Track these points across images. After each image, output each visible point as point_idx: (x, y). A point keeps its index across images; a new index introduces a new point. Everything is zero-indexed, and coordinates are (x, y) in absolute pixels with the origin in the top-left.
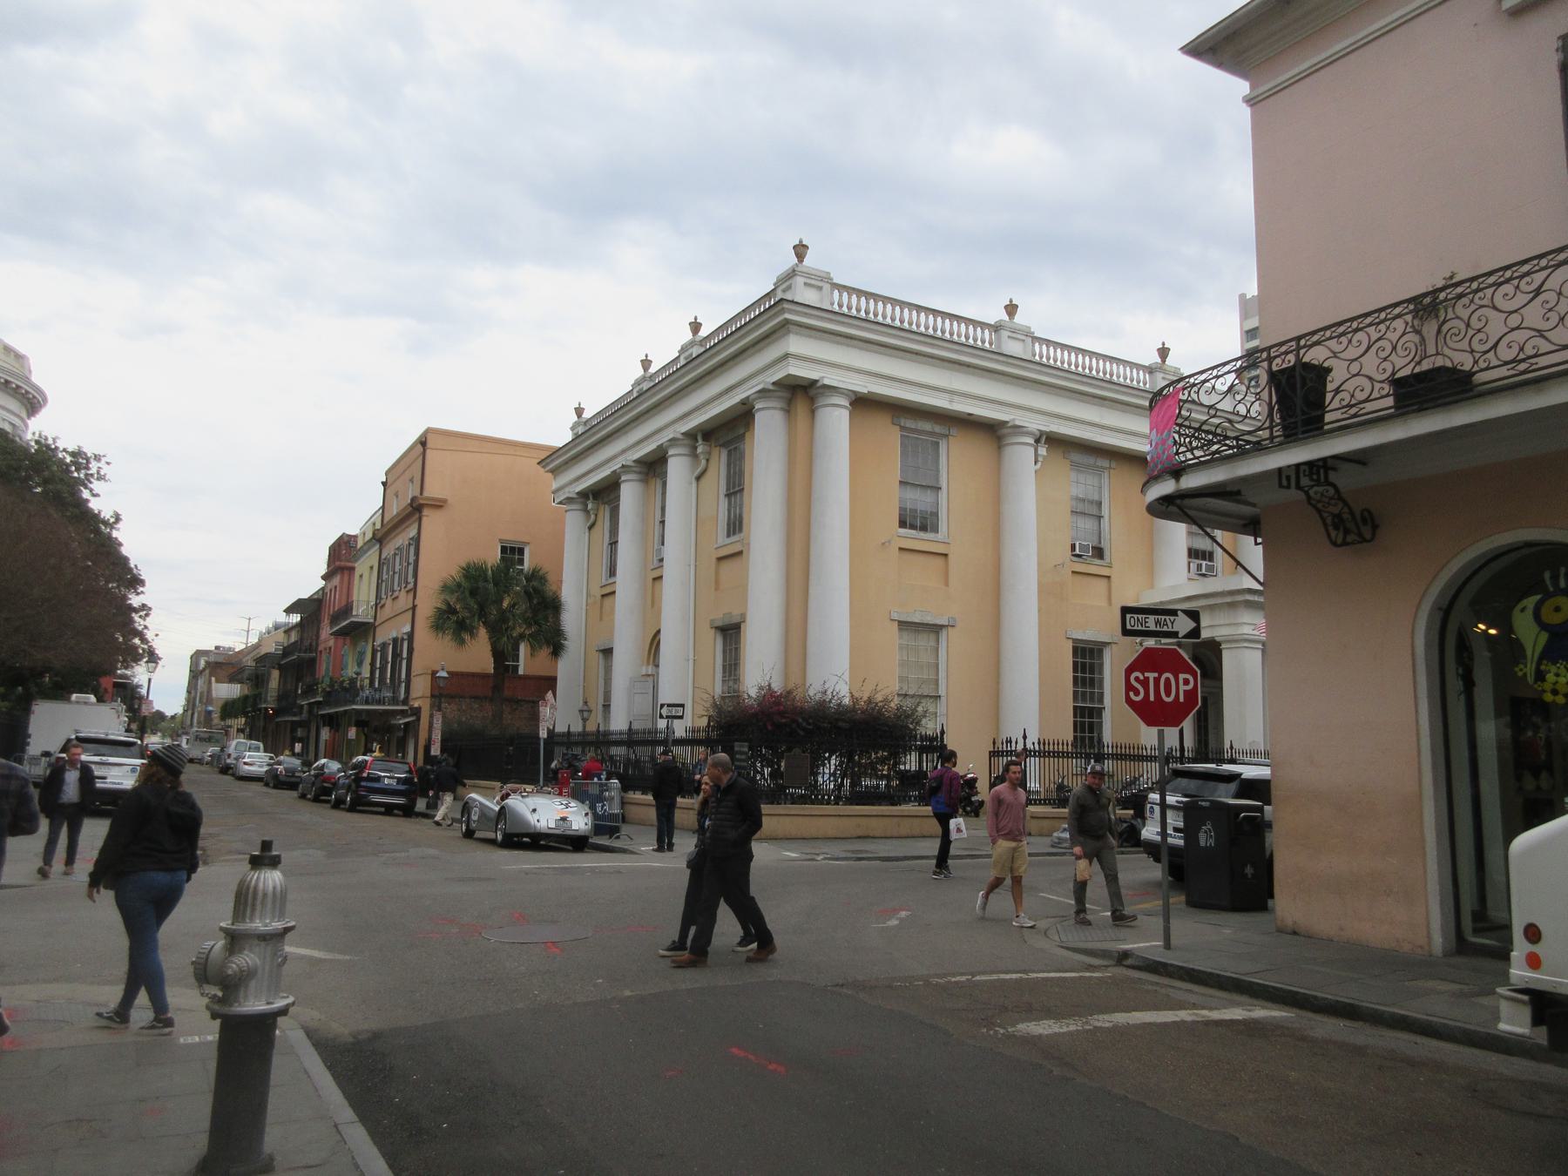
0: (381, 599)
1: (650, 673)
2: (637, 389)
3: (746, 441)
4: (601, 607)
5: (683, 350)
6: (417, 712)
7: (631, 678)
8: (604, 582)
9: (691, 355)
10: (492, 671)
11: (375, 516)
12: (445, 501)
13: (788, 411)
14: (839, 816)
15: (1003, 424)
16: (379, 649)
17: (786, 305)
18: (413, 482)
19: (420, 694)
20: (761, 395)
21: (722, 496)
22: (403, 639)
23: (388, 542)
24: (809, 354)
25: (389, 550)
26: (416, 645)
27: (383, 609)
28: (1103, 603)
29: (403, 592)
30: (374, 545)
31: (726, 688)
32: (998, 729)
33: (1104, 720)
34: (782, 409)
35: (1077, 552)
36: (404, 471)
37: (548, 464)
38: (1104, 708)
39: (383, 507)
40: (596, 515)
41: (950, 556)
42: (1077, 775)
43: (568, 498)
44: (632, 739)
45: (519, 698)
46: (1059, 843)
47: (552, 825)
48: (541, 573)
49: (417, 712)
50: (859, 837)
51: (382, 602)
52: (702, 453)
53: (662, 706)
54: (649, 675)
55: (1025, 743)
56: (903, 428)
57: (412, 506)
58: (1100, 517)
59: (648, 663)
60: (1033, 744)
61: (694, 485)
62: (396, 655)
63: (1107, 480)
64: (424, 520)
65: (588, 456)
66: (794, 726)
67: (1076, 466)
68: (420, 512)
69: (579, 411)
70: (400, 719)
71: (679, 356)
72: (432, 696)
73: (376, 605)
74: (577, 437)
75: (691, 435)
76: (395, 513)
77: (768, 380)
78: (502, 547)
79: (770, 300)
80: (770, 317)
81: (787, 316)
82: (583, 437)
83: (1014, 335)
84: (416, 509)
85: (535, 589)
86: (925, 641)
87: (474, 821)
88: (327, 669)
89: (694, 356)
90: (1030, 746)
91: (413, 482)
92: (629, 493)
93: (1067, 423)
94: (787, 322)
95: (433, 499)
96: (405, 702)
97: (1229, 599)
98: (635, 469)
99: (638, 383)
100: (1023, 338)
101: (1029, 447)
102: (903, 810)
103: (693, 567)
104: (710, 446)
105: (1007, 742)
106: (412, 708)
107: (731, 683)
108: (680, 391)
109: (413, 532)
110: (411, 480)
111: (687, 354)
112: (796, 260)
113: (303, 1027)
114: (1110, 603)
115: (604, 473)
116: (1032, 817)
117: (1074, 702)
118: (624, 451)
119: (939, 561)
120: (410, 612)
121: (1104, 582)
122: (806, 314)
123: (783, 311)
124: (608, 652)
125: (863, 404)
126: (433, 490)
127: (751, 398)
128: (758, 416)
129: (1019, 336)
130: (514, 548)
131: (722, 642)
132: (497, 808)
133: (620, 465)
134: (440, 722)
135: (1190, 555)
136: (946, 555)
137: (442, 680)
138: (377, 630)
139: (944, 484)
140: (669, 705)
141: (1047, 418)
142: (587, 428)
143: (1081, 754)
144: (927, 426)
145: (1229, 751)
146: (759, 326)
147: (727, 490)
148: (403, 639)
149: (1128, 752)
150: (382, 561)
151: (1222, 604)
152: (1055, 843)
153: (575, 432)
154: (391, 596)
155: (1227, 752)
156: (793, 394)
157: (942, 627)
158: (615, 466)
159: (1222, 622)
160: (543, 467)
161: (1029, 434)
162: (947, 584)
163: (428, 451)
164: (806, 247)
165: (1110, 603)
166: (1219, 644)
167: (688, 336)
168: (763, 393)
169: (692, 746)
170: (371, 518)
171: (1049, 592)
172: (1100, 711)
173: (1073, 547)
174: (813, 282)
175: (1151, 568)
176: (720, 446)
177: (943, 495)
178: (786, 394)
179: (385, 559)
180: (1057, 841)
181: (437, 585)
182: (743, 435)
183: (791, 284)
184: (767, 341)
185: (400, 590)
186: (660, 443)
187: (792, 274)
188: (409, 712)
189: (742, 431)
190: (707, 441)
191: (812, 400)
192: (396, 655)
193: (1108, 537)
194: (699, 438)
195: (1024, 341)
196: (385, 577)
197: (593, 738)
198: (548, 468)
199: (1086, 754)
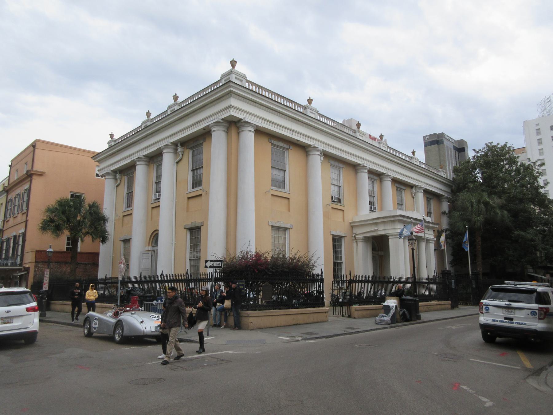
0: (7, 218)
1: (150, 250)
2: (144, 125)
3: (204, 145)
4: (123, 220)
5: (170, 107)
6: (27, 270)
7: (141, 252)
8: (124, 210)
9: (174, 109)
10: (65, 250)
11: (6, 180)
12: (44, 173)
13: (228, 132)
14: (286, 315)
15: (309, 146)
16: (5, 241)
17: (231, 84)
18: (27, 164)
19: (29, 261)
20: (215, 124)
21: (154, 184)
22: (19, 236)
23: (12, 192)
25: (12, 195)
26: (27, 238)
27: (8, 222)
28: (341, 220)
29: (20, 214)
30: (4, 194)
31: (192, 256)
33: (342, 267)
34: (225, 131)
35: (334, 200)
36: (22, 160)
37: (96, 158)
38: (342, 262)
39: (9, 177)
40: (120, 181)
41: (290, 199)
42: (335, 290)
43: (107, 173)
44: (141, 281)
45: (79, 262)
46: (381, 322)
47: (153, 330)
48: (96, 204)
49: (27, 270)
50: (294, 325)
51: (8, 219)
52: (180, 151)
53: (206, 262)
54: (149, 251)
55: (350, 277)
56: (273, 144)
57: (27, 174)
58: (339, 187)
59: (149, 246)
60: (353, 277)
61: (175, 165)
62: (15, 243)
63: (342, 173)
64: (33, 181)
65: (118, 154)
66: (266, 271)
67: (332, 166)
68: (31, 177)
69: (112, 136)
70: (18, 273)
71: (167, 110)
72: (36, 262)
73: (4, 221)
74: (110, 147)
75: (175, 144)
76: (16, 179)
77: (220, 117)
78: (71, 195)
79: (217, 85)
80: (222, 89)
81: (231, 89)
82: (113, 147)
83: (312, 111)
84: (29, 176)
85: (94, 212)
86: (280, 234)
87: (95, 328)
89: (175, 110)
91: (27, 164)
92: (140, 171)
94: (231, 92)
95: (36, 171)
96: (21, 265)
97: (393, 219)
98: (112, 174)
99: (144, 122)
100: (315, 113)
101: (318, 156)
102: (320, 310)
103: (174, 202)
104: (184, 149)
106: (25, 268)
107: (195, 253)
108: (171, 124)
109: (26, 186)
110: (26, 164)
111: (171, 109)
112: (231, 68)
115: (129, 161)
116: (356, 310)
117: (333, 260)
118: (138, 151)
119: (286, 201)
120: (25, 223)
121: (341, 212)
122: (239, 89)
123: (230, 86)
124: (127, 241)
125: (260, 132)
126: (38, 167)
127: (161, 148)
128: (213, 134)
129: (313, 112)
130: (77, 195)
131: (190, 235)
132: (113, 321)
133: (137, 157)
134: (48, 274)
135: (374, 203)
136: (288, 198)
137: (50, 253)
138: (4, 232)
139: (287, 169)
140: (211, 261)
141: (325, 145)
142: (116, 143)
143: (339, 282)
144: (281, 144)
146: (129, 141)
147: (192, 168)
148: (19, 236)
150: (8, 201)
151: (389, 221)
152: (379, 322)
153: (110, 144)
154: (21, 212)
156: (230, 125)
157: (287, 228)
158: (134, 157)
159: (389, 228)
160: (94, 159)
161: (319, 151)
162: (289, 211)
163: (36, 151)
164: (236, 62)
166: (388, 236)
167: (172, 101)
168: (217, 123)
169: (111, 284)
170: (2, 181)
171: (326, 216)
172: (341, 263)
173: (332, 197)
174: (239, 77)
175: (356, 207)
176: (189, 148)
177: (287, 174)
178: (226, 125)
179: (10, 200)
180: (380, 321)
181: (43, 208)
182: (133, 172)
183: (230, 77)
184: (220, 100)
185: (10, 218)
186: (159, 147)
187: (230, 72)
188: (23, 270)
189: (201, 142)
191: (238, 128)
192: (15, 243)
193: (342, 195)
195: (315, 114)
196: (9, 208)
197: (103, 281)
198: (96, 160)
199: (337, 281)
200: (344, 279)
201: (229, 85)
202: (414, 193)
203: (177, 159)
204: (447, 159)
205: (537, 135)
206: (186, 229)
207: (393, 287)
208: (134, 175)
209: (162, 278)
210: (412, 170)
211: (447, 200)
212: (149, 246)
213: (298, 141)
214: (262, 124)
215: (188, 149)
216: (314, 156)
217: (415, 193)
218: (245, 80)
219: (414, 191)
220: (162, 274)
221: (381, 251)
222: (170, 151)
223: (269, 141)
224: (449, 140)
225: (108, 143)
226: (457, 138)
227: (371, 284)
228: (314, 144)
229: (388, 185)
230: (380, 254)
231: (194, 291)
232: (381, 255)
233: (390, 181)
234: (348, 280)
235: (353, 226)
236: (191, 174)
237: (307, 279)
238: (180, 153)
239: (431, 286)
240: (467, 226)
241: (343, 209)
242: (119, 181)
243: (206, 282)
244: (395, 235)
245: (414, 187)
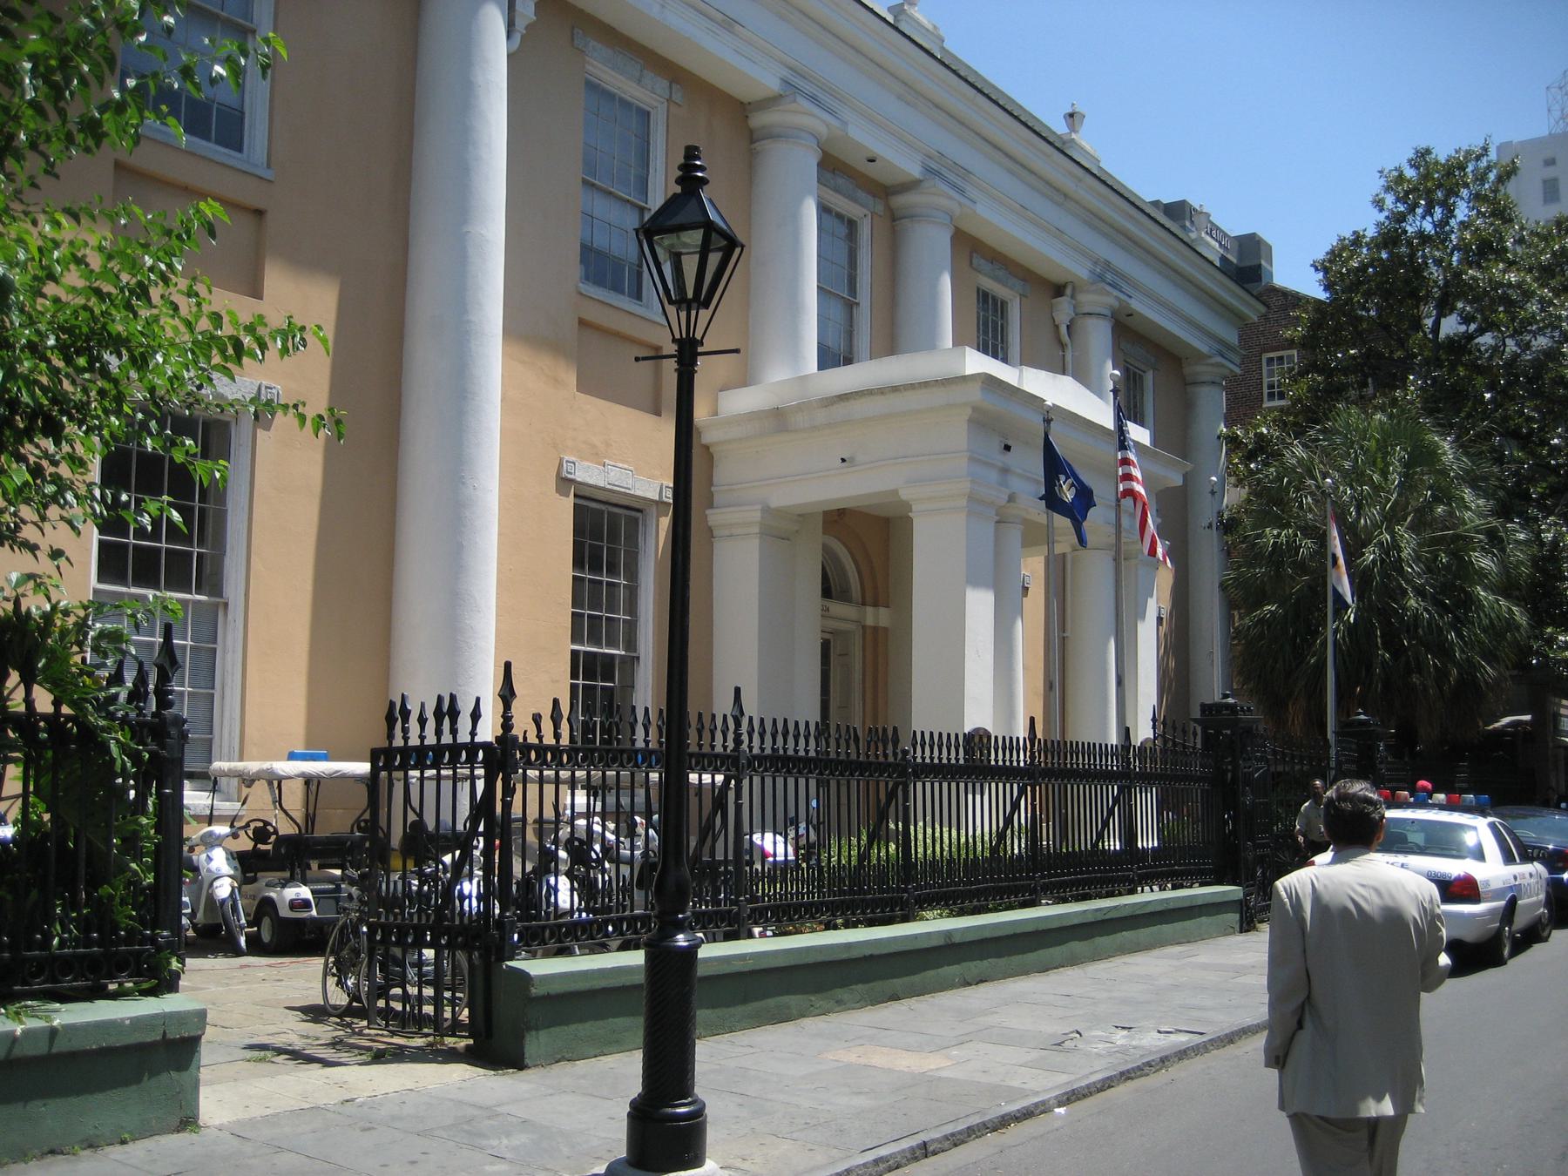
32: (875, 718)
38: (638, 658)
60: (537, 719)
88: (593, 66)
90: (522, 726)
105: (439, 715)
113: (1431, 880)
136: (259, 213)
149: (549, 740)
205: (1555, 180)
207: (888, 804)
221: (876, 605)
230: (870, 621)
232: (875, 629)
234: (486, 746)
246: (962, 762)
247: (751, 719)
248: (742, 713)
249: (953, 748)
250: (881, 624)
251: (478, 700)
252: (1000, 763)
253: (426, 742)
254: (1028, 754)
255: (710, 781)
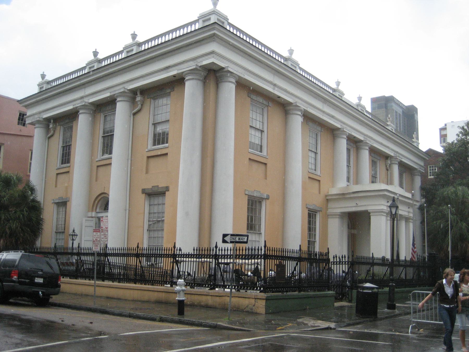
1: (93, 216)
13: (205, 81)
17: (216, 26)
21: (101, 138)
24: (93, 91)
28: (316, 191)
41: (268, 165)
54: (92, 217)
61: (132, 117)
93: (319, 111)
114: (320, 193)
119: (263, 167)
122: (227, 34)
123: (214, 29)
145: (215, 249)
155: (213, 250)
158: (78, 104)
161: (300, 110)
165: (320, 193)
166: (369, 213)
190: (142, 95)
194: (138, 93)
200: (345, 260)
201: (213, 27)
202: (388, 165)
203: (133, 110)
204: (402, 127)
206: (144, 194)
208: (73, 125)
209: (78, 251)
210: (390, 138)
211: (420, 174)
212: (92, 211)
213: (279, 97)
214: (244, 75)
215: (150, 99)
216: (295, 115)
217: (390, 165)
218: (227, 22)
219: (389, 162)
220: (138, 247)
222: (125, 100)
223: (248, 95)
224: (399, 104)
225: (39, 85)
226: (406, 102)
227: (295, 262)
228: (296, 102)
229: (365, 155)
231: (305, 275)
233: (367, 149)
235: (328, 200)
236: (151, 128)
237: (312, 258)
238: (139, 103)
239: (408, 268)
240: (449, 205)
241: (319, 180)
242: (52, 132)
243: (116, 254)
244: (382, 212)
245: (389, 158)
246: (307, 257)
247: (268, 247)
248: (266, 246)
249: (282, 252)
250: (353, 230)
251: (217, 243)
252: (305, 257)
253: (228, 254)
254: (299, 254)
255: (247, 262)
